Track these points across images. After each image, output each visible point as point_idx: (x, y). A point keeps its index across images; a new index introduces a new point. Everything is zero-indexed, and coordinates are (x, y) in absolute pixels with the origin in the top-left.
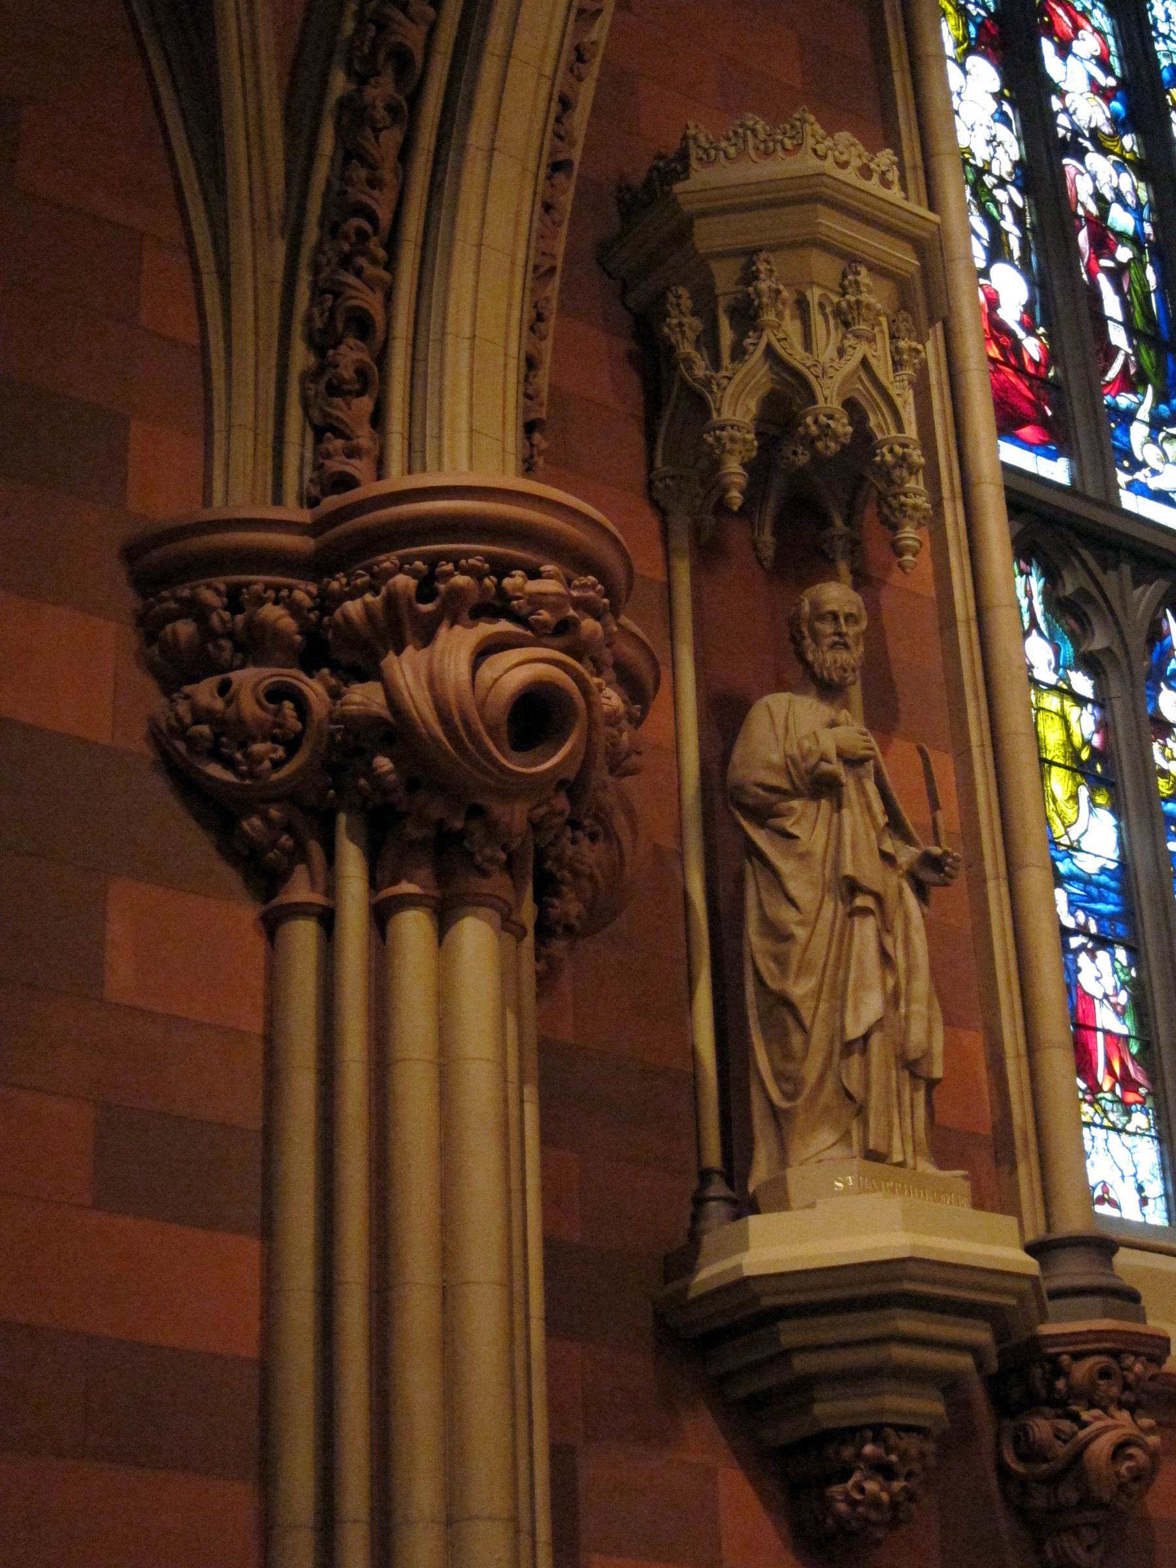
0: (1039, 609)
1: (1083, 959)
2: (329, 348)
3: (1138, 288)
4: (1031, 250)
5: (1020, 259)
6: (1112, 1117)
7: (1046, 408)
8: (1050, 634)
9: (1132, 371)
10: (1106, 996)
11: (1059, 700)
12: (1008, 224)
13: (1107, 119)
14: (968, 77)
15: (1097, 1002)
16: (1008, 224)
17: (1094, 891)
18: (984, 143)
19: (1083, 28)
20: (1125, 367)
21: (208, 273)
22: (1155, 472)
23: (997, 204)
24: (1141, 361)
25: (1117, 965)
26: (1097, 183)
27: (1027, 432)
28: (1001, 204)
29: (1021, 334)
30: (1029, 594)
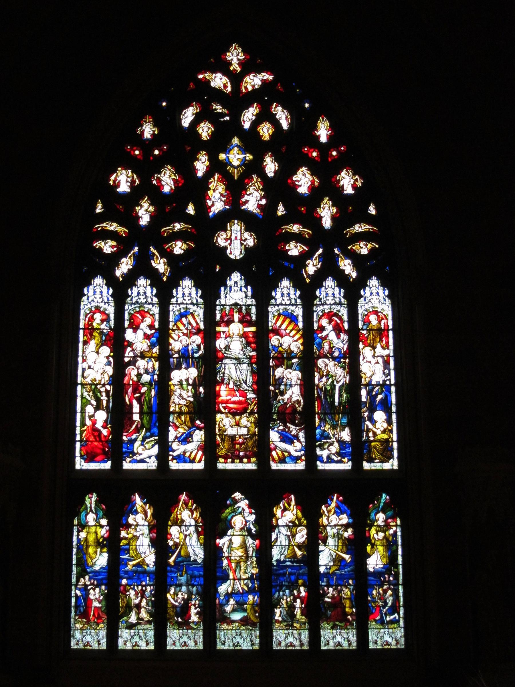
0: (93, 506)
1: (91, 591)
2: (333, 566)
3: (147, 398)
4: (110, 402)
5: (106, 407)
6: (93, 626)
7: (316, 402)
8: (96, 512)
9: (139, 426)
10: (96, 598)
11: (226, 537)
12: (104, 398)
13: (148, 346)
14: (99, 355)
15: (93, 601)
16: (104, 398)
17: (98, 574)
18: (100, 374)
19: (146, 317)
20: (137, 425)
21: (190, 525)
22: (140, 454)
23: (101, 392)
24: (143, 422)
25: (101, 590)
26: (139, 370)
27: (98, 458)
28: (102, 392)
29: (102, 429)
30: (91, 503)
